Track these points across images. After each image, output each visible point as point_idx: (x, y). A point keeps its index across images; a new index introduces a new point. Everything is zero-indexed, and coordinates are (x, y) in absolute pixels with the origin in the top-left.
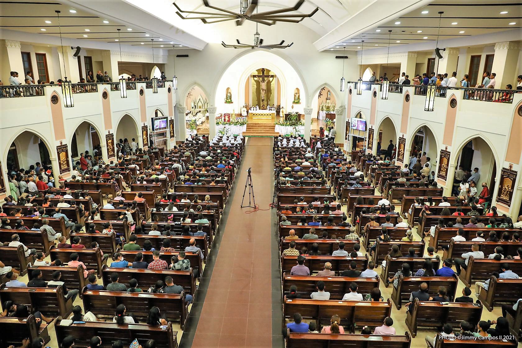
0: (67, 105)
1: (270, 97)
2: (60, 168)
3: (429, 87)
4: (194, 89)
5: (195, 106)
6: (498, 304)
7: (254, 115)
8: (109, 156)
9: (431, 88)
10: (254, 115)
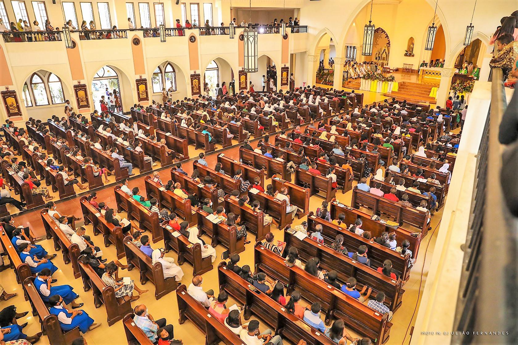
0: (69, 47)
1: (475, 53)
2: (240, 86)
3: (283, 24)
4: (381, 38)
5: (379, 57)
6: (376, 262)
7: (430, 73)
8: (283, 84)
9: (367, 30)
10: (427, 73)
